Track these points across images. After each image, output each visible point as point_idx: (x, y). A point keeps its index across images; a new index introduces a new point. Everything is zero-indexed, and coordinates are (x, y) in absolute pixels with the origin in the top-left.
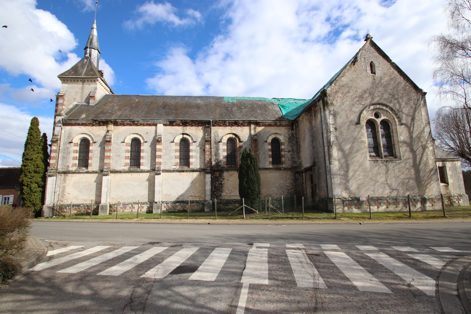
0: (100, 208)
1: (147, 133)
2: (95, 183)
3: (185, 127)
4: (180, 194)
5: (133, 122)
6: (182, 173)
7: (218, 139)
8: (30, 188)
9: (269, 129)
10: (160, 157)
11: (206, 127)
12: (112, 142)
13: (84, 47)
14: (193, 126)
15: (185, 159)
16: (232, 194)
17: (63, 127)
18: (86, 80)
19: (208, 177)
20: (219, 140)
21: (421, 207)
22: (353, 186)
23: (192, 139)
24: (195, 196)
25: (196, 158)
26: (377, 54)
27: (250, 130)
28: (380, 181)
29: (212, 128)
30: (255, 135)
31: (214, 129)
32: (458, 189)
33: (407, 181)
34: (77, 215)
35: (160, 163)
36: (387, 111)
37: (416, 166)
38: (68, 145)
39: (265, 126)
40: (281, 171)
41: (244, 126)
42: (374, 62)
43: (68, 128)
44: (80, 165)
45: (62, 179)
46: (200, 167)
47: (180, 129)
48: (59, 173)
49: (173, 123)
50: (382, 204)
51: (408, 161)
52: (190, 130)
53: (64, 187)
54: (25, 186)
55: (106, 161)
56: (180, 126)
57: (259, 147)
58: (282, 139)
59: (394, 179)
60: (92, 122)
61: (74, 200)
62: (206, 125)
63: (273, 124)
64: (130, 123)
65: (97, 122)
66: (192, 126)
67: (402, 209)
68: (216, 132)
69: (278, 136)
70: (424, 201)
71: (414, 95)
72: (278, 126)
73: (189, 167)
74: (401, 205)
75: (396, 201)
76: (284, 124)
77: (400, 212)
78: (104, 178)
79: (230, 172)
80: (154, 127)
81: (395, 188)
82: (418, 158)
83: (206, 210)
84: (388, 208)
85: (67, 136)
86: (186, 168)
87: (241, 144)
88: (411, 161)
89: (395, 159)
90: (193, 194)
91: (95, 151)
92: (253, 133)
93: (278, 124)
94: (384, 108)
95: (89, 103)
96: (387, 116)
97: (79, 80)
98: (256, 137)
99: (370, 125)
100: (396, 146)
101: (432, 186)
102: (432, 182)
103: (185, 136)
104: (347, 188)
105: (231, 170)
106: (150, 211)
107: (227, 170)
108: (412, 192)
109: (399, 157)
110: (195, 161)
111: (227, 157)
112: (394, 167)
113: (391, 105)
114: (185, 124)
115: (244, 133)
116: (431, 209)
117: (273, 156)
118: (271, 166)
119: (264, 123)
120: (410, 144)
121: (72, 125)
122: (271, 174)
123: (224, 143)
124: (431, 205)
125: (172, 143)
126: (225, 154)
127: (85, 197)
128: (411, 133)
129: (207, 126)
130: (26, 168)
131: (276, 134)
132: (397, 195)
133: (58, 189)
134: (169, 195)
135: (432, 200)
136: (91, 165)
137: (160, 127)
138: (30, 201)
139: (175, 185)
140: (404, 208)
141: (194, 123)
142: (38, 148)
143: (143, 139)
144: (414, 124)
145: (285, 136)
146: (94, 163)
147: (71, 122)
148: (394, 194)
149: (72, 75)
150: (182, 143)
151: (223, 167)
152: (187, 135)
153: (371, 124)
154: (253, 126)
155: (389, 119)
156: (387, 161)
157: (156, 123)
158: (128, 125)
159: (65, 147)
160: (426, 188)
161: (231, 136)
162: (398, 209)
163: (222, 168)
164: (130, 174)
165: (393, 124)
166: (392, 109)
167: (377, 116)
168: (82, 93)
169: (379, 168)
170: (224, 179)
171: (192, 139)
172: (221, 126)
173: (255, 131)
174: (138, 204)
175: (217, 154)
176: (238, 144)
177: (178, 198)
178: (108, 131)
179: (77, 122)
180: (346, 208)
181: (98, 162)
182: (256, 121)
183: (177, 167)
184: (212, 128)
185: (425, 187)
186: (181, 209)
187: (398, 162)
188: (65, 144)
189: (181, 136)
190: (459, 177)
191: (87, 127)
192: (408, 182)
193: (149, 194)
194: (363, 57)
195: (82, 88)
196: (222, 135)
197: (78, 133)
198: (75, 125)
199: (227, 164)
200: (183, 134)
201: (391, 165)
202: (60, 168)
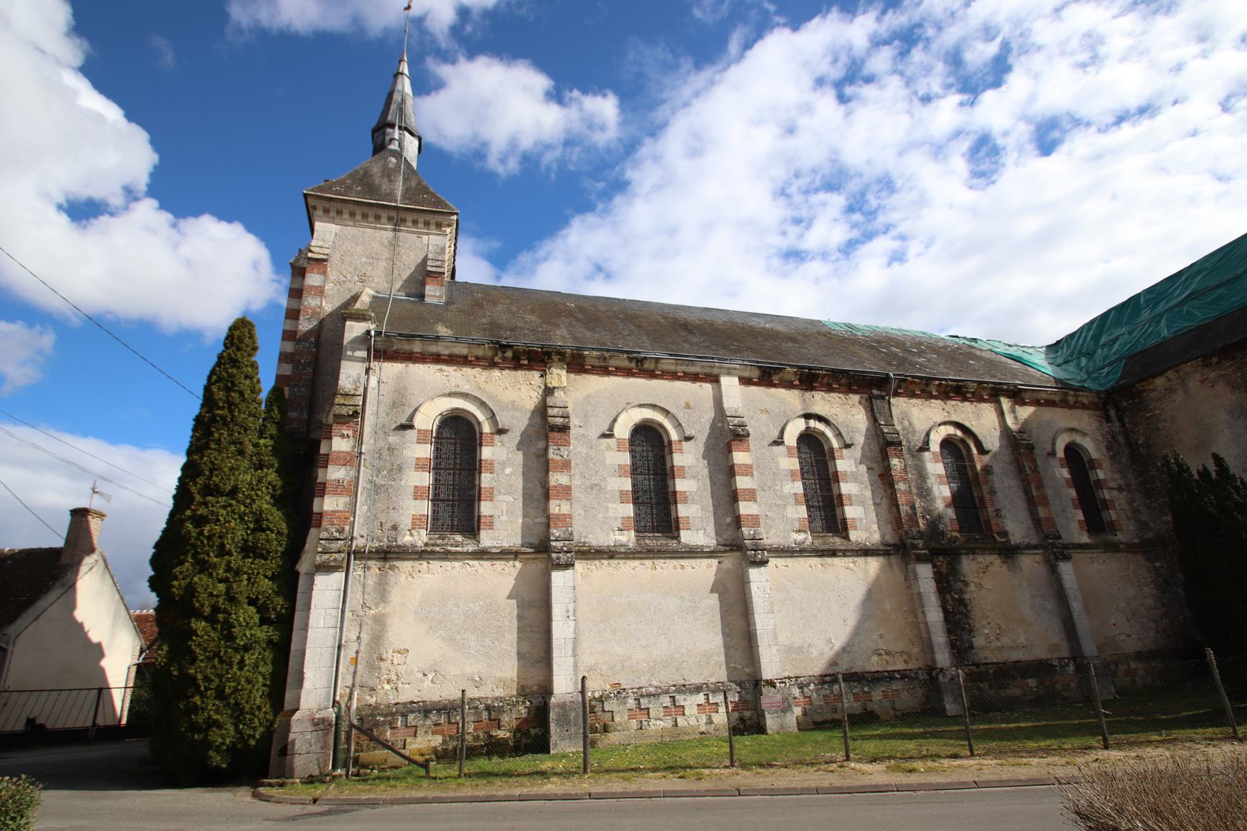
0: (552, 716)
1: (688, 406)
2: (514, 602)
3: (808, 394)
5: (640, 361)
6: (829, 560)
7: (918, 440)
8: (228, 625)
9: (1048, 414)
10: (751, 495)
12: (573, 431)
13: (373, 123)
15: (826, 509)
16: (1006, 640)
17: (375, 365)
18: (410, 217)
19: (925, 572)
24: (887, 652)
25: (862, 503)
27: (1001, 414)
31: (900, 405)
34: (444, 756)
35: (755, 521)
38: (393, 439)
40: (1118, 555)
41: (982, 400)
43: (391, 369)
44: (437, 525)
45: (371, 582)
46: (883, 536)
47: (791, 399)
48: (360, 554)
49: (770, 375)
52: (822, 402)
53: (380, 621)
54: (199, 615)
55: (555, 507)
58: (1091, 447)
60: (489, 354)
61: (427, 683)
63: (1057, 398)
64: (626, 364)
65: (509, 354)
66: (830, 389)
69: (1079, 439)
72: (1070, 407)
73: (847, 538)
76: (1085, 401)
78: (558, 577)
79: (980, 558)
80: (708, 387)
83: (951, 707)
85: (387, 400)
86: (837, 542)
90: (882, 645)
91: (504, 464)
93: (1071, 399)
95: (422, 296)
97: (384, 214)
106: (748, 722)
110: (863, 517)
111: (957, 501)
119: (1035, 395)
121: (410, 357)
125: (775, 448)
127: (474, 668)
129: (875, 392)
130: (206, 530)
131: (1072, 430)
133: (350, 633)
134: (800, 649)
136: (491, 526)
137: (730, 383)
138: (221, 695)
139: (815, 612)
141: (838, 381)
142: (256, 445)
143: (679, 426)
145: (1095, 440)
146: (503, 516)
147: (406, 347)
149: (358, 194)
151: (953, 540)
152: (820, 419)
154: (1006, 403)
157: (715, 371)
158: (628, 373)
159: (381, 444)
161: (951, 430)
164: (648, 563)
168: (392, 260)
174: (698, 689)
175: (925, 493)
177: (833, 663)
178: (548, 391)
179: (433, 348)
181: (520, 513)
182: (1015, 385)
183: (806, 538)
186: (856, 707)
188: (380, 431)
191: (468, 371)
193: (727, 647)
195: (394, 245)
196: (926, 427)
197: (434, 391)
198: (423, 358)
200: (808, 416)
202: (362, 534)
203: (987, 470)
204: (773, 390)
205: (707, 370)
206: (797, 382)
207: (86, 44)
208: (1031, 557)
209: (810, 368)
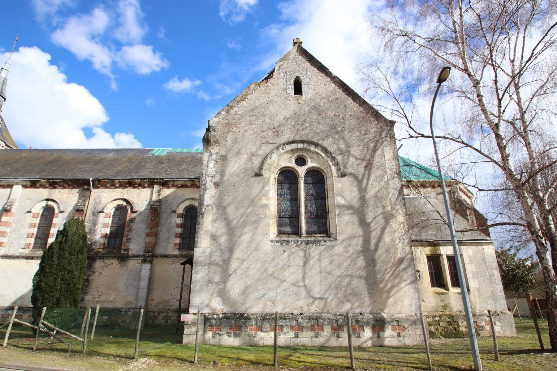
4: (19, 295)
9: (182, 191)
11: (84, 190)
14: (65, 188)
20: (100, 210)
21: (372, 338)
22: (235, 287)
23: (59, 207)
26: (308, 65)
28: (290, 280)
29: (93, 190)
30: (156, 201)
31: (95, 192)
32: (491, 301)
33: (347, 280)
36: (317, 153)
37: (369, 253)
39: (177, 187)
41: (144, 187)
42: (301, 77)
47: (44, 193)
50: (285, 330)
51: (354, 241)
56: (47, 188)
57: (162, 220)
59: (317, 278)
62: (83, 185)
63: (189, 184)
67: (328, 340)
68: (99, 197)
70: (379, 324)
71: (373, 127)
74: (327, 331)
75: (316, 322)
77: (322, 348)
79: (107, 261)
81: (318, 296)
82: (374, 235)
84: (297, 336)
87: (134, 215)
88: (360, 241)
89: (327, 239)
92: (155, 198)
94: (312, 148)
96: (318, 163)
98: (157, 204)
99: (286, 177)
100: (331, 215)
101: (402, 292)
102: (403, 285)
103: (50, 203)
104: (223, 294)
105: (108, 258)
107: (102, 258)
108: (357, 304)
109: (334, 236)
112: (321, 253)
113: (324, 144)
114: (53, 184)
115: (141, 199)
116: (395, 342)
117: (181, 236)
118: (176, 252)
120: (360, 212)
122: (174, 265)
123: (107, 214)
124: (395, 333)
125: (28, 214)
126: (108, 231)
128: (362, 191)
129: (86, 187)
131: (192, 199)
132: (323, 309)
135: (398, 323)
137: (18, 189)
140: (334, 338)
144: (369, 175)
148: (315, 309)
150: (46, 213)
152: (54, 201)
153: (287, 177)
155: (322, 168)
156: (307, 243)
157: (11, 184)
160: (388, 297)
161: (121, 202)
162: (319, 341)
163: (95, 253)
165: (328, 175)
166: (325, 150)
167: (301, 161)
169: (289, 256)
170: (94, 272)
171: (59, 207)
172: (108, 188)
173: (159, 195)
176: (130, 216)
180: (209, 335)
182: (162, 179)
184: (93, 190)
185: (385, 295)
187: (330, 243)
189: (44, 203)
190: (492, 275)
192: (349, 284)
194: (284, 70)
199: (104, 248)
200: (48, 200)
201: (315, 251)
203: (132, 220)
204: (37, 189)
205: (8, 184)
206: (48, 186)
207: (186, 78)
208: (136, 261)
209: (52, 179)
